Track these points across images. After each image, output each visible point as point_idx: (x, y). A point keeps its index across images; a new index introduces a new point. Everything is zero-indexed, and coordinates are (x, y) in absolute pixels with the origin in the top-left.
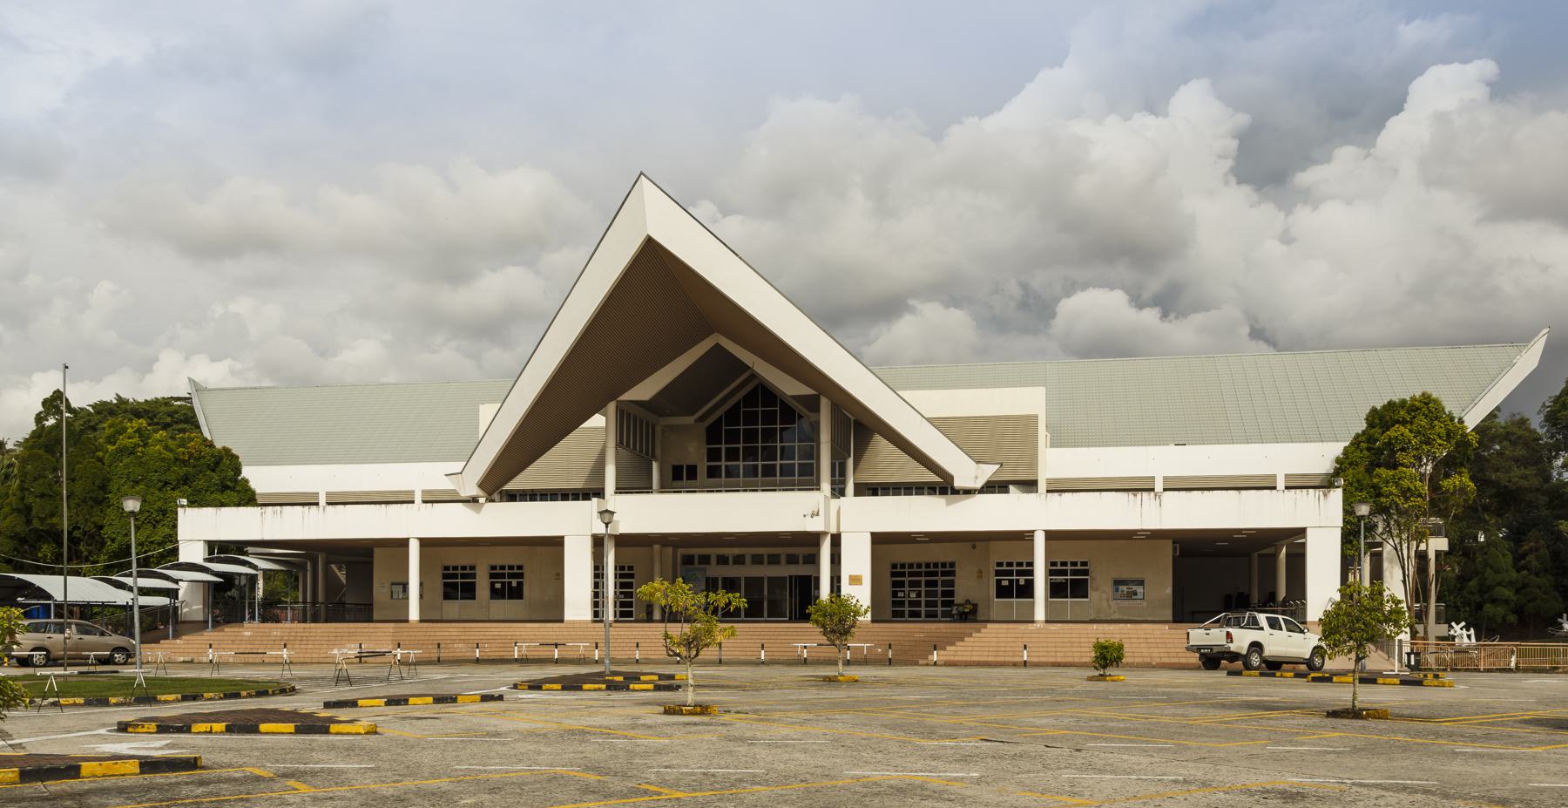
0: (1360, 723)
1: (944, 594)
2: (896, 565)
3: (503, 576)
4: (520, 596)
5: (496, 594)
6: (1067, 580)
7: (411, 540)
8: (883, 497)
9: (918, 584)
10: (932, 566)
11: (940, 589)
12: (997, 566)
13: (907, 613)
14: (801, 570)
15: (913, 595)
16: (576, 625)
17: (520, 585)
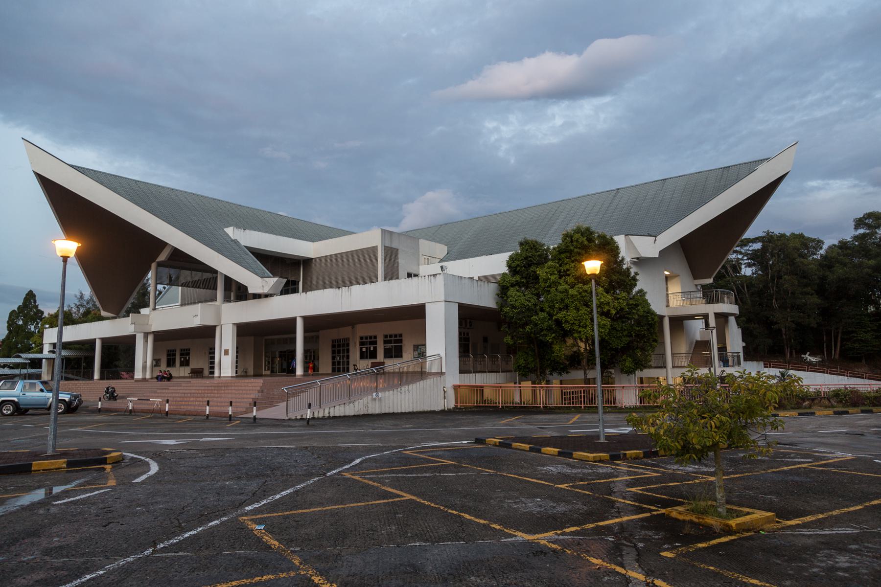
0: (94, 448)
2: (387, 336)
6: (392, 346)
7: (297, 318)
8: (286, 296)
10: (398, 336)
14: (287, 348)
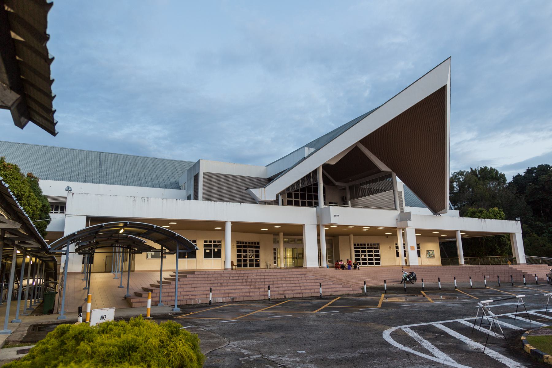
1: (376, 255)
3: (210, 246)
4: (220, 257)
5: (207, 255)
9: (365, 252)
10: (217, 242)
11: (373, 254)
12: (205, 242)
13: (374, 263)
15: (363, 256)
16: (311, 270)
17: (219, 251)
